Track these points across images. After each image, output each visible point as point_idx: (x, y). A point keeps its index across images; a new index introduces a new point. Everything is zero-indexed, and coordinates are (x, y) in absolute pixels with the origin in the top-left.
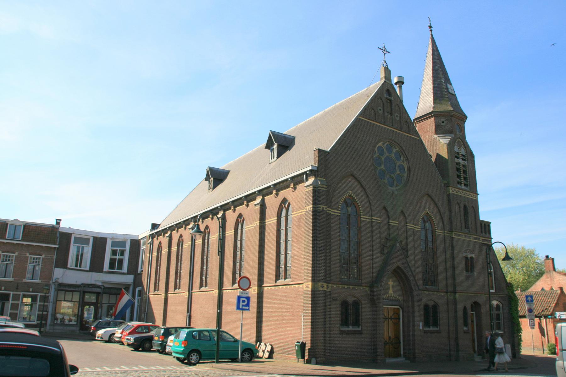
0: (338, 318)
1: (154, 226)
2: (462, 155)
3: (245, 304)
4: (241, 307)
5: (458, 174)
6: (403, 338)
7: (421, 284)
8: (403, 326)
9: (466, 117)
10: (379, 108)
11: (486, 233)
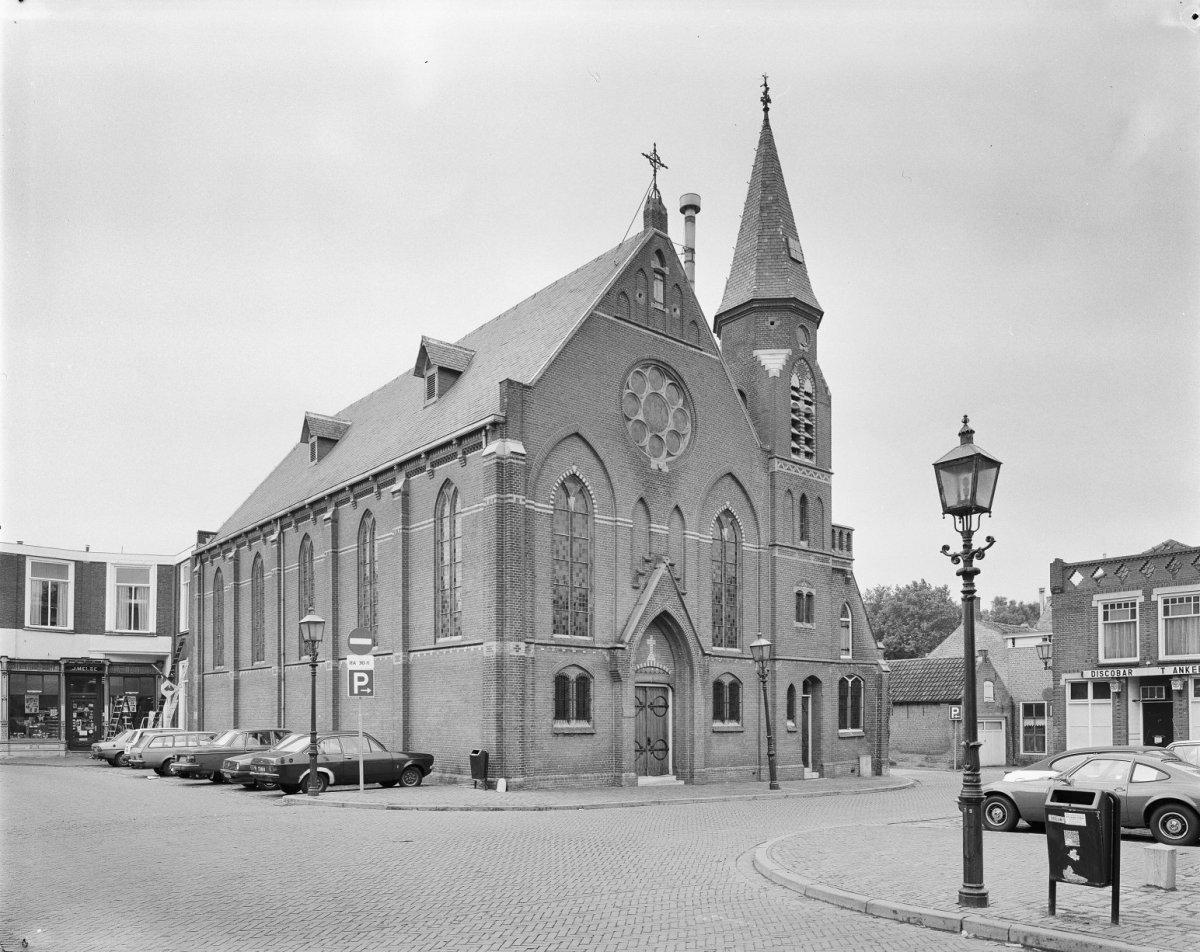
0: (550, 707)
1: (203, 536)
2: (807, 394)
3: (363, 683)
4: (356, 691)
5: (794, 431)
6: (674, 736)
7: (707, 641)
8: (674, 718)
9: (821, 314)
10: (639, 291)
11: (841, 548)
